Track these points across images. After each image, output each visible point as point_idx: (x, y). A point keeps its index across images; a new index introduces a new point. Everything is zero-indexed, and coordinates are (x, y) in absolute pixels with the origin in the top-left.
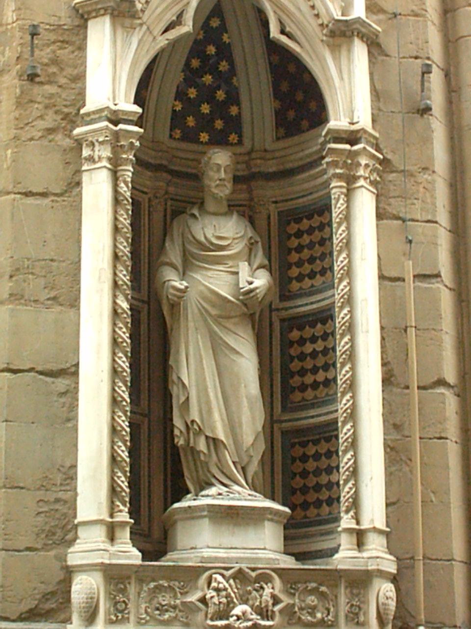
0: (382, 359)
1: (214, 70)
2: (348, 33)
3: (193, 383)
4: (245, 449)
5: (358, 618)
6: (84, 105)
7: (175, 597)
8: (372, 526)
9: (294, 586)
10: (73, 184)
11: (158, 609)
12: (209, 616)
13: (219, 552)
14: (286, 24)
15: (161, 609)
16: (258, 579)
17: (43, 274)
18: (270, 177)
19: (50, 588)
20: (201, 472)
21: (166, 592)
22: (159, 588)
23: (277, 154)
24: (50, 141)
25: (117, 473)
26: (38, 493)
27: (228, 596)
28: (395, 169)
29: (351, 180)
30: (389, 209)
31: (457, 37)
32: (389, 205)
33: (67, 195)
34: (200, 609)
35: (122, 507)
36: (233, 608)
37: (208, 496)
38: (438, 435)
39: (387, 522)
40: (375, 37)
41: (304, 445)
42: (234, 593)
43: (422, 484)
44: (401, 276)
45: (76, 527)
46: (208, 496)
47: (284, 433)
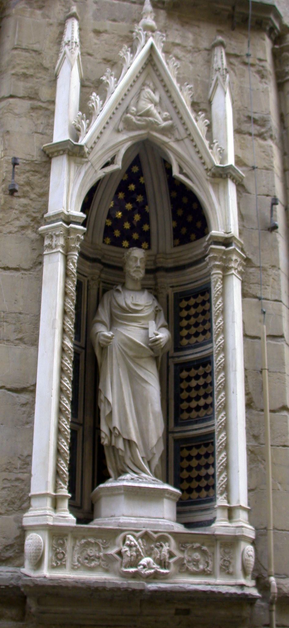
0: (246, 390)
1: (133, 201)
2: (224, 176)
3: (116, 401)
4: (150, 449)
5: (228, 570)
6: (47, 212)
7: (99, 550)
10: (37, 263)
11: (86, 559)
12: (123, 565)
13: (132, 520)
14: (183, 168)
15: (89, 558)
17: (14, 322)
18: (168, 270)
19: (10, 542)
20: (119, 464)
21: (92, 546)
22: (88, 544)
23: (175, 256)
24: (23, 235)
25: (60, 461)
26: (4, 473)
27: (137, 551)
28: (254, 266)
29: (225, 269)
30: (251, 291)
32: (250, 288)
33: (33, 270)
34: (116, 560)
35: (63, 485)
36: (141, 560)
37: (124, 480)
38: (282, 444)
40: (241, 180)
41: (189, 448)
42: (142, 548)
43: (273, 478)
44: (258, 335)
45: (30, 498)
46: (124, 480)
47: (176, 441)
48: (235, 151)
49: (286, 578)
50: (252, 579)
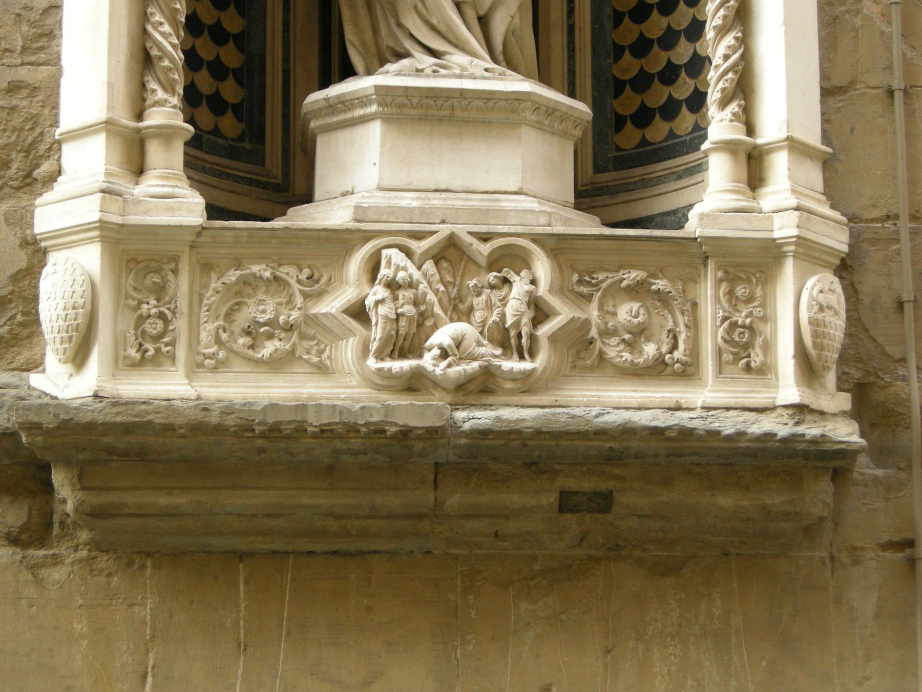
16: (496, 262)
22: (249, 284)
35: (161, 94)
42: (436, 292)
45: (57, 145)
50: (840, 389)
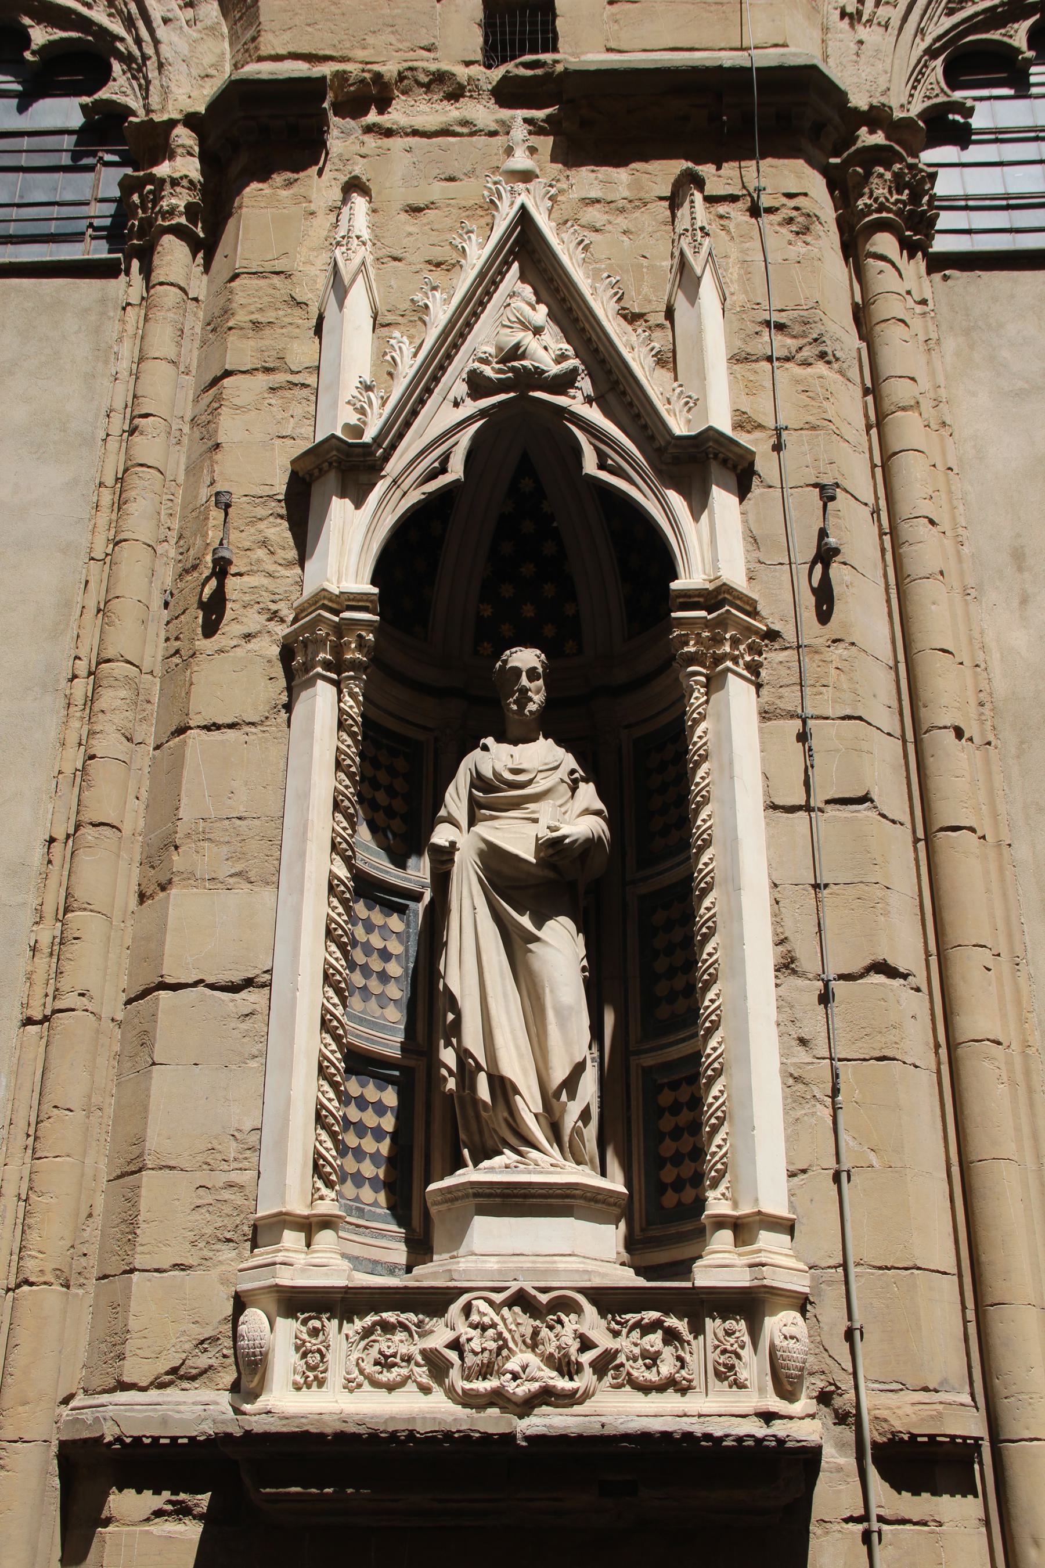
8: (756, 1210)
9: (618, 1318)
15: (385, 1362)
31: (891, 452)
36: (508, 1358)
38: (878, 1054)
39: (790, 1202)
42: (510, 1331)
48: (734, 398)
49: (901, 1390)
